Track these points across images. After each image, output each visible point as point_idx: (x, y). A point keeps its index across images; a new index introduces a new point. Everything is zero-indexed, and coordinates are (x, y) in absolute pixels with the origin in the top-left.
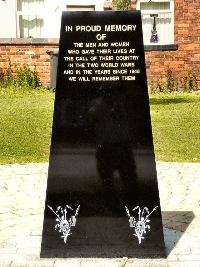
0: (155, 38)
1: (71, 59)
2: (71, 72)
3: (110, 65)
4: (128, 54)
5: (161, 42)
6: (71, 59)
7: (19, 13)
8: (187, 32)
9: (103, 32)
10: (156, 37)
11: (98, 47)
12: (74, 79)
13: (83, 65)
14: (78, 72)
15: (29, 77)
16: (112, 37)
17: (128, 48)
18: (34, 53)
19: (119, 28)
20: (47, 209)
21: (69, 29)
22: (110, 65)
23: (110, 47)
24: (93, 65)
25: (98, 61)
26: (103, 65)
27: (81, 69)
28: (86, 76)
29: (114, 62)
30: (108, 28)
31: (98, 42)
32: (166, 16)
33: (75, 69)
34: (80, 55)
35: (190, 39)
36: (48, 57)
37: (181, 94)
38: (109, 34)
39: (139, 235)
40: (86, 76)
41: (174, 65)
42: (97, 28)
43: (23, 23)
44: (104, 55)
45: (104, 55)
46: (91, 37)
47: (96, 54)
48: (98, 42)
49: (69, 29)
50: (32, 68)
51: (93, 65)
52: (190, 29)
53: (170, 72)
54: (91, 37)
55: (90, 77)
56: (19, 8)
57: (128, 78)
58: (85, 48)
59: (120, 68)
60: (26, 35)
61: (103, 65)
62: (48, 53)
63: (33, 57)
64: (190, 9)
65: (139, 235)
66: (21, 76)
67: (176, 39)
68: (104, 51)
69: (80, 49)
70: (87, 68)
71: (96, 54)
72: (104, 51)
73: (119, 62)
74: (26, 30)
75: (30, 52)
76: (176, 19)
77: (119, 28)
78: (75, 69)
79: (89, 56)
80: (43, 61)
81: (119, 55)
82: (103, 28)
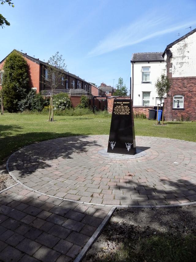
0: (178, 106)
1: (115, 109)
2: (115, 112)
3: (124, 111)
4: (127, 109)
5: (180, 108)
6: (115, 109)
7: (143, 99)
8: (187, 105)
9: (122, 103)
10: (179, 106)
11: (121, 107)
12: (116, 114)
13: (118, 111)
14: (117, 112)
15: (143, 116)
16: (124, 105)
17: (128, 107)
18: (145, 110)
19: (126, 103)
20: (109, 142)
21: (115, 103)
22: (124, 111)
23: (124, 107)
24: (120, 111)
25: (121, 110)
26: (122, 111)
27: (117, 112)
28: (118, 113)
29: (124, 110)
30: (123, 103)
31: (121, 106)
32: (182, 101)
33: (116, 111)
34: (117, 108)
35: (189, 107)
36: (149, 111)
37: (181, 122)
38: (124, 104)
39: (128, 149)
40: (118, 113)
41: (183, 114)
42: (121, 103)
43: (144, 102)
44: (122, 109)
45: (122, 109)
46: (120, 105)
47: (121, 108)
48: (121, 106)
49: (115, 103)
50: (144, 113)
51: (120, 111)
52: (188, 104)
53: (182, 116)
54: (120, 105)
55: (119, 113)
56: (143, 98)
57: (127, 114)
58: (118, 107)
59: (126, 111)
60: (145, 105)
61: (122, 111)
62: (148, 110)
63: (145, 111)
64: (188, 99)
65: (128, 149)
66: (141, 115)
67: (184, 107)
68: (122, 108)
69: (117, 107)
70: (119, 111)
71: (121, 108)
72: (122, 108)
73: (126, 110)
74: (145, 104)
75: (144, 109)
76: (184, 102)
77: (126, 103)
78: (116, 111)
79: (119, 109)
80: (147, 112)
81: (126, 109)
82: (122, 103)
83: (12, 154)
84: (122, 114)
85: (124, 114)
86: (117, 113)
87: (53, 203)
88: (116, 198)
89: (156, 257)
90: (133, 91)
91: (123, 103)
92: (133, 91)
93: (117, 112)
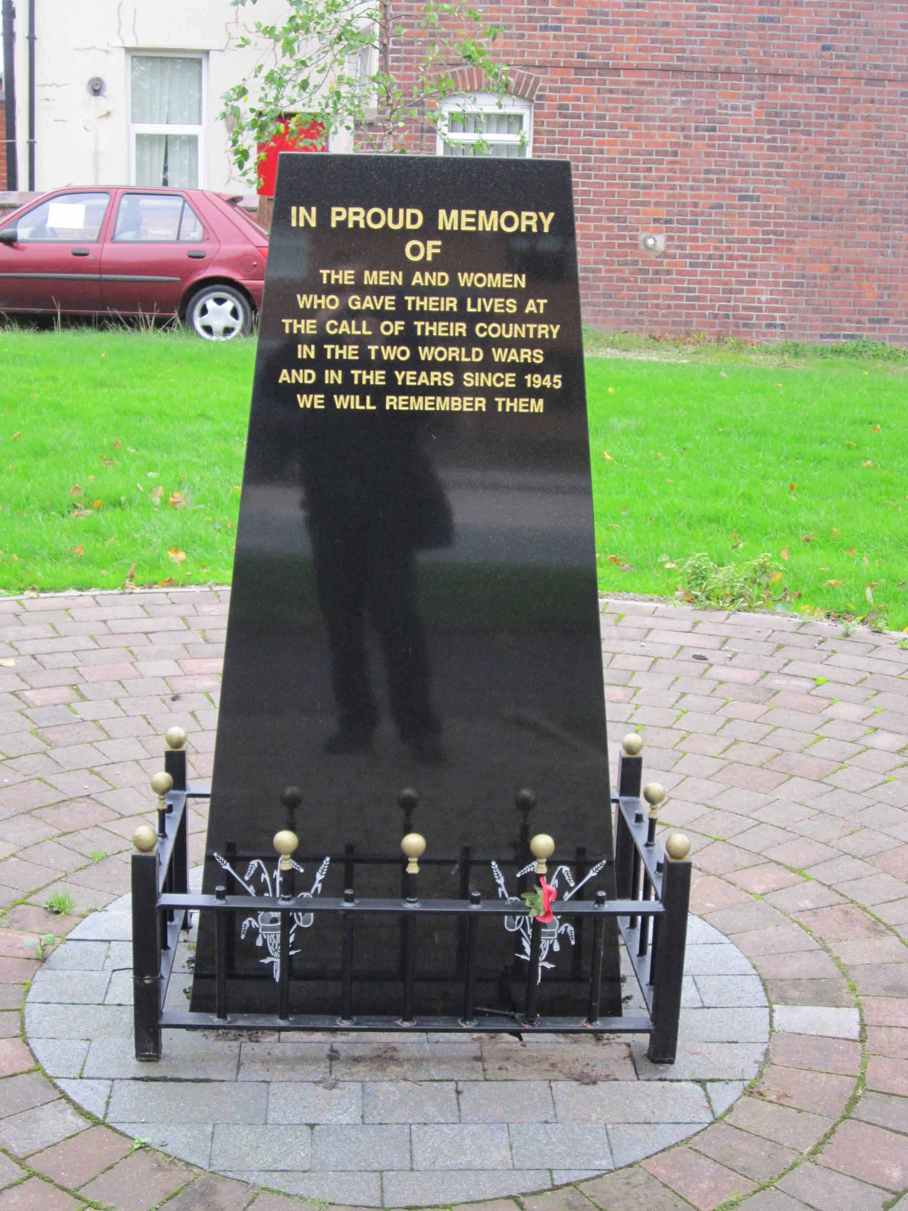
1: (308, 327)
2: (306, 376)
3: (453, 353)
4: (521, 318)
6: (308, 327)
9: (429, 231)
12: (316, 401)
13: (350, 352)
14: (333, 377)
17: (522, 296)
23: (453, 289)
25: (409, 338)
26: (426, 353)
27: (345, 365)
28: (362, 390)
30: (447, 220)
31: (409, 269)
33: (320, 363)
34: (345, 314)
38: (448, 237)
40: (362, 390)
47: (401, 312)
48: (409, 269)
51: (389, 353)
55: (378, 394)
57: (519, 405)
58: (361, 289)
59: (488, 366)
61: (426, 353)
68: (429, 304)
70: (365, 363)
71: (401, 312)
72: (429, 304)
73: (487, 344)
78: (320, 363)
81: (489, 317)
83: (564, 878)
84: (419, 404)
85: (519, 405)
86: (330, 391)
87: (162, 1149)
88: (775, 1061)
89: (642, 1200)
90: (32, 39)
91: (447, 220)
92: (32, 39)
93: (333, 377)
